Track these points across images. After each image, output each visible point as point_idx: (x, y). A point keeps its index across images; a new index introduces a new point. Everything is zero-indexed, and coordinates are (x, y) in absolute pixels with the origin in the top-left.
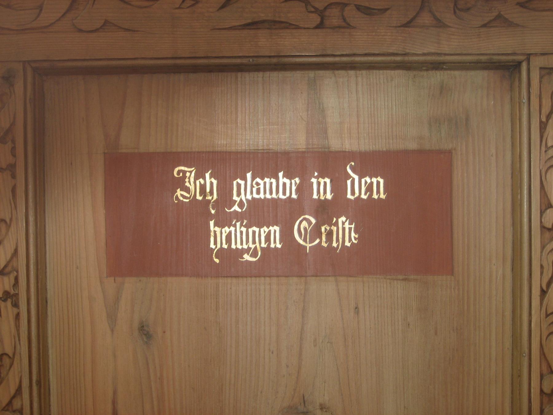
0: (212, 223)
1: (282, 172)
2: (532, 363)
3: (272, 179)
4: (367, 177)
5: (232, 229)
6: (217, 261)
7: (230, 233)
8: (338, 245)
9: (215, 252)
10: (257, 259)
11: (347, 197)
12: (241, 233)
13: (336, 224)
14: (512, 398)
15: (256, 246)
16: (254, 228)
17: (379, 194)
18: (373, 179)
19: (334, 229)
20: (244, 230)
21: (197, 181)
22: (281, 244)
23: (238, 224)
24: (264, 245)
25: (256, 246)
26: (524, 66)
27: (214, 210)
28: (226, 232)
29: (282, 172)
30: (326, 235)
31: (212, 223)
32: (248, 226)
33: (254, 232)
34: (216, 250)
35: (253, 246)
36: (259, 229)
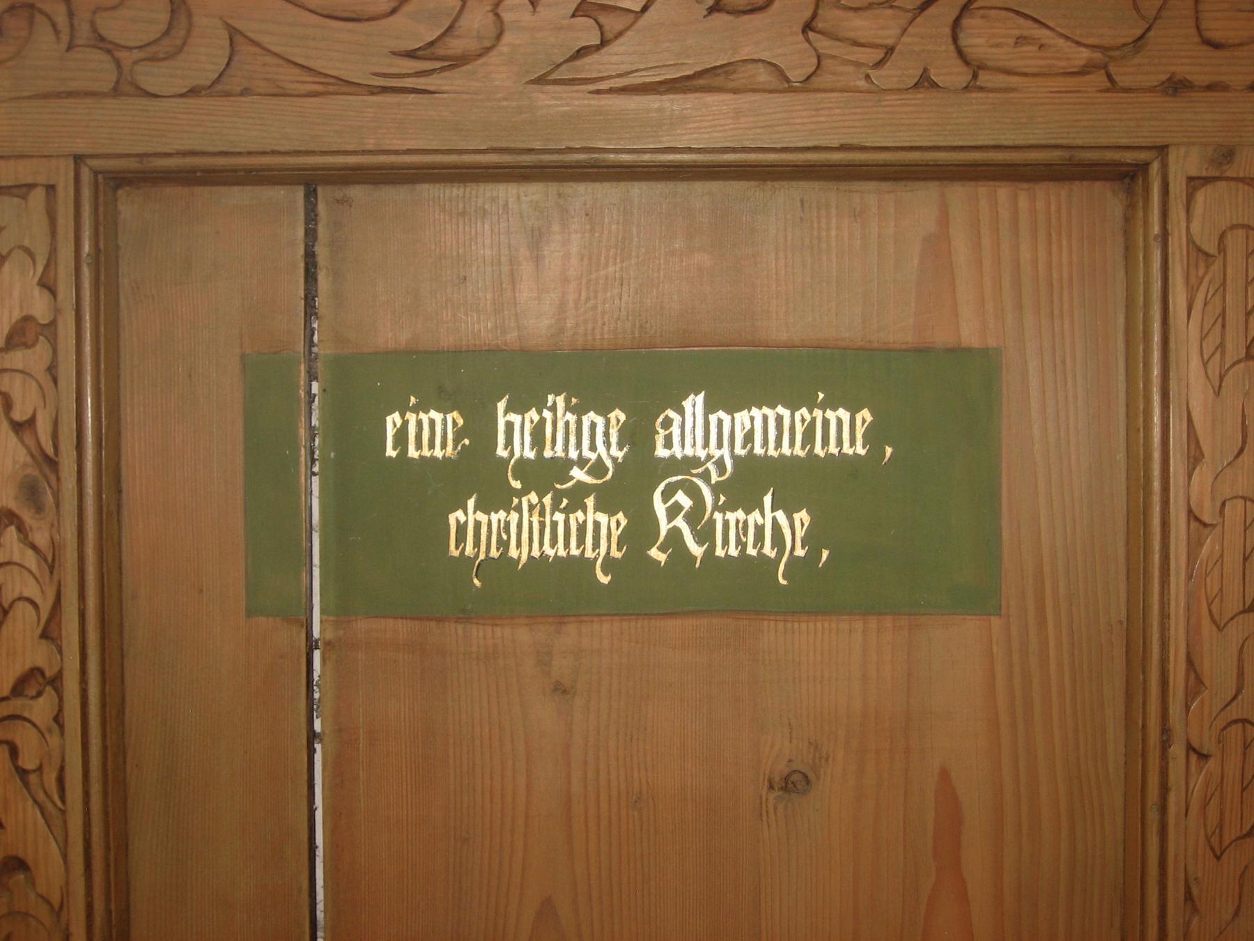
0: (501, 405)
1: (703, 394)
2: (810, 144)
3: (421, 413)
4: (779, 406)
5: (514, 516)
6: (783, 582)
7: (543, 421)
8: (510, 450)
9: (510, 467)
10: (600, 482)
11: (393, 459)
12: (554, 525)
13: (519, 509)
14: (1128, 677)
15: (599, 455)
16: (721, 414)
17: (583, 547)
18: (814, 412)
19: (547, 414)
20: (571, 418)
21: (796, 413)
22: (397, 451)
23: (560, 401)
24: (740, 451)
25: (599, 455)
26: (1155, 166)
27: (395, 450)
28: (395, 425)
29: (703, 393)
30: (619, 431)
31: (501, 405)
32: (580, 411)
33: (720, 422)
34: (512, 462)
35: (593, 456)
36: (442, 415)
